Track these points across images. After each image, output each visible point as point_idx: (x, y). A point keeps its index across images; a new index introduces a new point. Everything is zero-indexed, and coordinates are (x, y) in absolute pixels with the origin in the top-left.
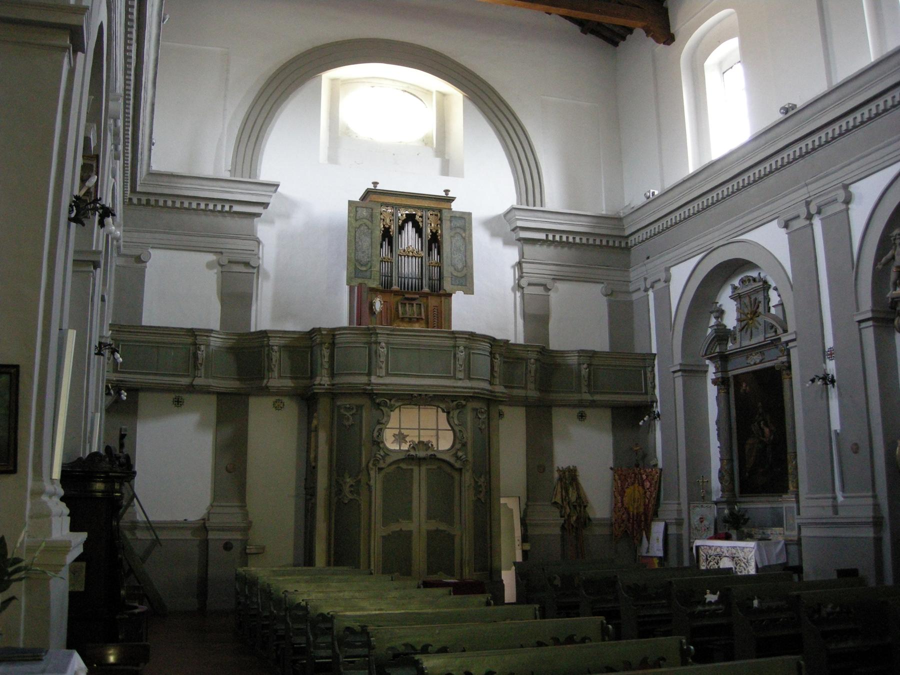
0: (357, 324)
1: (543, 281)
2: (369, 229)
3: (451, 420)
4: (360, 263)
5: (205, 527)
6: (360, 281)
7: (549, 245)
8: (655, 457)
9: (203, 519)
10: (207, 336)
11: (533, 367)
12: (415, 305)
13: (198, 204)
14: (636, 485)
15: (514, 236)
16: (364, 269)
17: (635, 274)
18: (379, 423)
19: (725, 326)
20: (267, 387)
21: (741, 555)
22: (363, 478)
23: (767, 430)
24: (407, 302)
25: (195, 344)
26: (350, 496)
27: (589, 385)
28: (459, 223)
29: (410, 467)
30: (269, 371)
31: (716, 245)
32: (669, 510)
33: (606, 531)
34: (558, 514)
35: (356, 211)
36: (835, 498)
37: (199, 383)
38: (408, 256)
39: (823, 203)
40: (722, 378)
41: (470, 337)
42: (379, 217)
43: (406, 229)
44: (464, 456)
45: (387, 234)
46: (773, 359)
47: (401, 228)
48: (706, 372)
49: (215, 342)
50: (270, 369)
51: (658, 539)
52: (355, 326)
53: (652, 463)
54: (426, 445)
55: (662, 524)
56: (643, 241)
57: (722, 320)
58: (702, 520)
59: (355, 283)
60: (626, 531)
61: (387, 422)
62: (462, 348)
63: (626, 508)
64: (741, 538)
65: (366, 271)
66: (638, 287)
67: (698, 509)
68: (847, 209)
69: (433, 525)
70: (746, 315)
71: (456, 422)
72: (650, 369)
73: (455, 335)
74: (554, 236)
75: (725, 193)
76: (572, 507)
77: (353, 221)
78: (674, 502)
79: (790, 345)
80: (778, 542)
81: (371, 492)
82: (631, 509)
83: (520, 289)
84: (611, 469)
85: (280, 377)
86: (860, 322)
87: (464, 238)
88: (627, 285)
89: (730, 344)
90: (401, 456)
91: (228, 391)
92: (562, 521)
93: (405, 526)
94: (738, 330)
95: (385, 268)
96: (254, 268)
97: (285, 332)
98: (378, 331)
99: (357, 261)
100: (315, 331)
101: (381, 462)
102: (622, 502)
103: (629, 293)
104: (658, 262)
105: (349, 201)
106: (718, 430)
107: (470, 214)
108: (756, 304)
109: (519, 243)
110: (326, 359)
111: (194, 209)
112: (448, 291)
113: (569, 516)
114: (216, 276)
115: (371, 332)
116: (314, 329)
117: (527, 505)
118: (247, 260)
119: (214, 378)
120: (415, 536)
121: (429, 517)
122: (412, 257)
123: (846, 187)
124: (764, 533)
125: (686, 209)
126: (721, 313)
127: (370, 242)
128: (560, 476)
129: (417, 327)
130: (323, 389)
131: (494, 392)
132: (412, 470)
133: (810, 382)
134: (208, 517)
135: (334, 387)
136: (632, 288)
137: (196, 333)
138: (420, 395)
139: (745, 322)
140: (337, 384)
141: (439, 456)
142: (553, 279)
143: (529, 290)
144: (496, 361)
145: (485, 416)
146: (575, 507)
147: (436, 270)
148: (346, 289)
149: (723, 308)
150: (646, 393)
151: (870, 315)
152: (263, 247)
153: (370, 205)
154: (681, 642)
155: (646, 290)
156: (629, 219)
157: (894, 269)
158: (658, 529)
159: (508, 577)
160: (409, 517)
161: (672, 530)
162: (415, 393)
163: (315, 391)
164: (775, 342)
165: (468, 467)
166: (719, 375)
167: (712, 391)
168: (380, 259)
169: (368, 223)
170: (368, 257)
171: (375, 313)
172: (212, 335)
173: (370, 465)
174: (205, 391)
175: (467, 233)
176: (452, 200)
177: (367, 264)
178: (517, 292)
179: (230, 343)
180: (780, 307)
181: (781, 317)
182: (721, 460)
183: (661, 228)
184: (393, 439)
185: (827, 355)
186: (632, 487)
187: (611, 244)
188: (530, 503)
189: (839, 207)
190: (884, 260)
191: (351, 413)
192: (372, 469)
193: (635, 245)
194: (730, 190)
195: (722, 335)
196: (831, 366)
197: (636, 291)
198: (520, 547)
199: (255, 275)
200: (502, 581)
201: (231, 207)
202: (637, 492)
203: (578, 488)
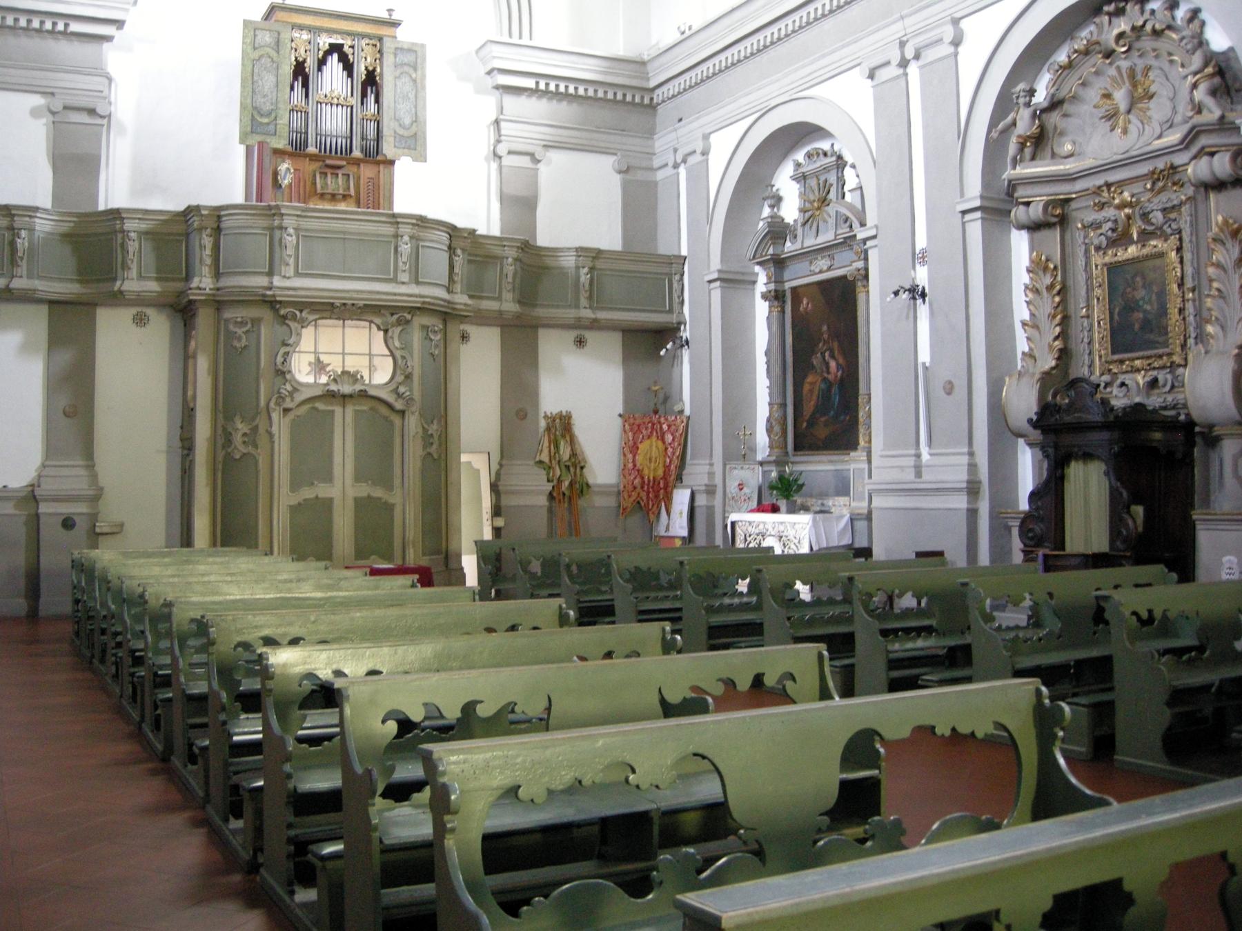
0: (257, 201)
1: (529, 149)
2: (273, 61)
3: (390, 342)
4: (259, 112)
5: (34, 497)
6: (259, 138)
7: (540, 97)
8: (681, 400)
9: (33, 485)
10: (30, 217)
11: (510, 269)
12: (340, 176)
13: (16, 20)
14: (654, 438)
15: (490, 82)
16: (265, 120)
17: (662, 143)
18: (285, 344)
19: (783, 220)
20: (121, 292)
21: (791, 533)
22: (261, 423)
23: (833, 364)
24: (329, 171)
25: (11, 228)
26: (243, 449)
27: (590, 298)
28: (408, 58)
29: (330, 408)
30: (123, 269)
31: (773, 103)
32: (697, 473)
33: (611, 502)
34: (545, 478)
35: (255, 36)
36: (918, 456)
37: (20, 286)
38: (331, 105)
39: (922, 44)
40: (776, 291)
41: (419, 223)
42: (289, 46)
43: (329, 63)
44: (408, 393)
45: (299, 70)
46: (844, 266)
47: (322, 63)
48: (754, 282)
49: (43, 225)
50: (125, 266)
51: (681, 513)
52: (254, 203)
53: (677, 408)
54: (353, 377)
55: (688, 492)
56: (673, 96)
57: (778, 209)
58: (741, 487)
59: (254, 140)
60: (638, 502)
61: (298, 343)
62: (406, 238)
63: (638, 471)
64: (792, 510)
65: (268, 124)
66: (664, 162)
67: (736, 472)
68: (956, 54)
69: (364, 490)
70: (812, 202)
71: (397, 344)
72: (677, 277)
73: (395, 219)
74: (547, 85)
75: (790, 28)
76: (563, 467)
77: (249, 49)
78: (703, 462)
79: (869, 244)
80: (842, 516)
81: (273, 443)
82: (646, 472)
83: (497, 159)
84: (620, 415)
85: (141, 277)
86: (964, 213)
87: (415, 81)
88: (651, 159)
89: (788, 244)
90: (318, 392)
91: (62, 298)
92: (549, 487)
93: (323, 491)
94: (799, 225)
95: (297, 120)
96: (102, 117)
97: (146, 212)
98: (283, 211)
99: (255, 108)
100: (191, 211)
101: (288, 400)
102: (634, 461)
103: (652, 169)
104: (695, 125)
105: (245, 21)
106: (768, 363)
107: (423, 46)
108: (826, 188)
109: (497, 93)
110: (208, 252)
111: (10, 27)
112: (390, 157)
113: (560, 481)
114: (44, 129)
115: (273, 212)
116: (189, 207)
117: (501, 465)
118: (91, 106)
119: (40, 278)
120: (337, 504)
121: (359, 477)
122: (337, 105)
123: (956, 22)
124: (823, 505)
125: (734, 50)
126: (777, 200)
127: (274, 80)
128: (548, 424)
129: (342, 206)
130: (202, 295)
131: (453, 303)
132: (333, 412)
133: (893, 296)
134: (39, 480)
135: (219, 292)
136: (656, 163)
137: (13, 212)
138: (344, 304)
139: (810, 213)
140: (225, 288)
141: (372, 392)
142: (545, 146)
143: (508, 161)
144: (457, 258)
145: (439, 337)
146: (568, 467)
147: (373, 125)
148: (241, 149)
149: (781, 193)
150: (671, 311)
151: (977, 203)
152: (116, 86)
153: (277, 27)
154: (664, 630)
155: (676, 166)
156: (656, 64)
157: (1014, 140)
158: (681, 498)
159: (470, 564)
160: (328, 478)
161: (701, 501)
162: (338, 302)
163: (191, 298)
164: (849, 241)
165: (414, 409)
166: (772, 286)
167: (762, 309)
168: (290, 107)
169: (273, 54)
170: (272, 104)
171: (280, 186)
172: (38, 215)
173: (272, 405)
174: (27, 298)
175: (419, 72)
176: (395, 24)
177: (270, 113)
178: (492, 162)
179: (65, 228)
180: (859, 192)
181: (859, 207)
182: (770, 404)
183: (699, 77)
184: (309, 369)
185: (918, 258)
186: (647, 443)
187: (629, 98)
188: (504, 462)
189: (946, 49)
190: (1000, 126)
191: (245, 329)
192: (275, 410)
193: (663, 101)
194: (797, 24)
195: (778, 231)
196: (922, 276)
197: (660, 168)
198: (490, 522)
199: (105, 128)
200: (462, 569)
201: (66, 25)
202: (654, 448)
203: (572, 441)
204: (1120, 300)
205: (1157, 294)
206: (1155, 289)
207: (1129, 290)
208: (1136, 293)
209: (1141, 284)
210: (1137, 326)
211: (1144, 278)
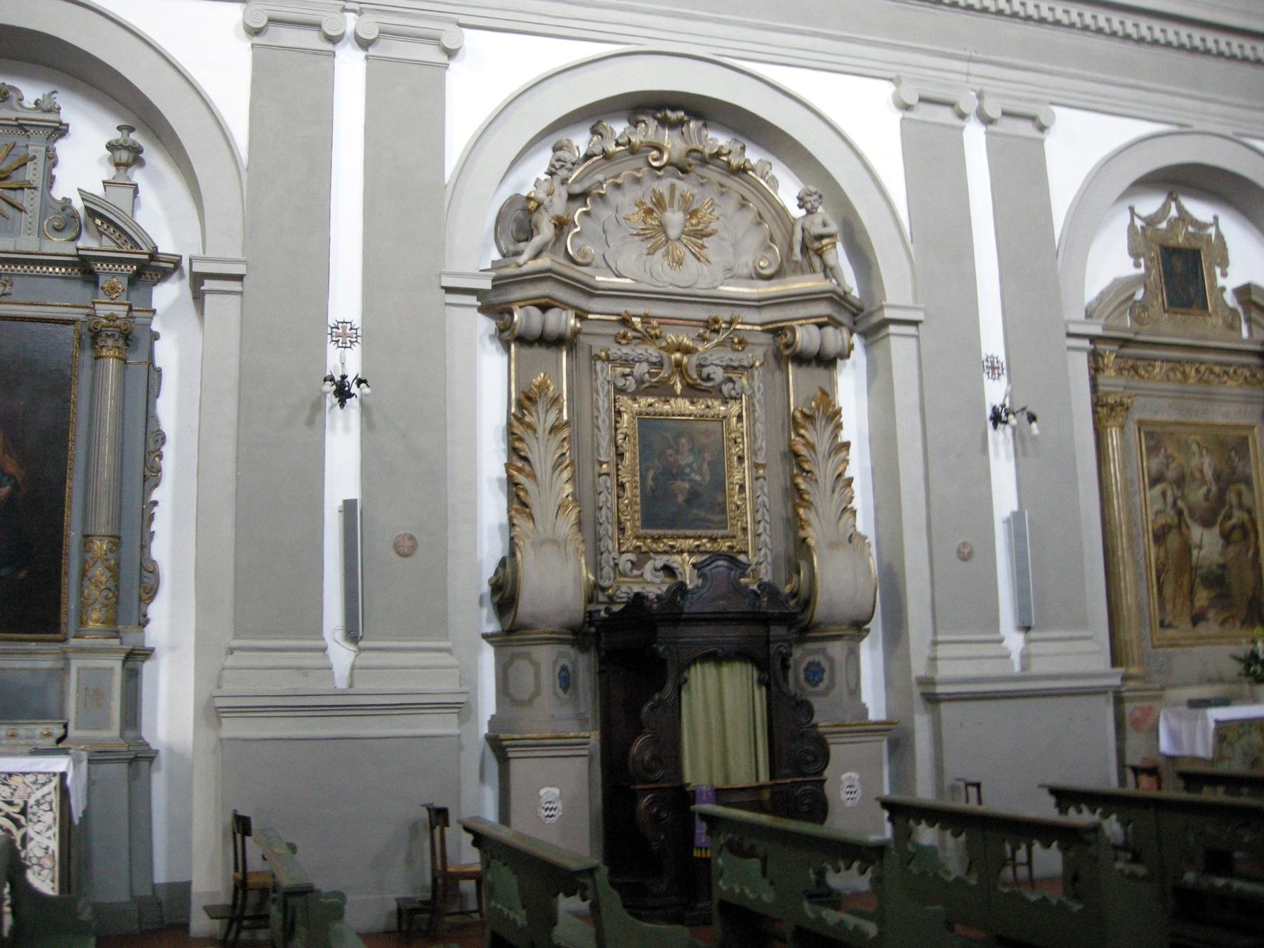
204: (656, 461)
205: (709, 463)
206: (707, 456)
207: (670, 451)
208: (680, 458)
209: (687, 447)
210: (680, 498)
211: (691, 439)
